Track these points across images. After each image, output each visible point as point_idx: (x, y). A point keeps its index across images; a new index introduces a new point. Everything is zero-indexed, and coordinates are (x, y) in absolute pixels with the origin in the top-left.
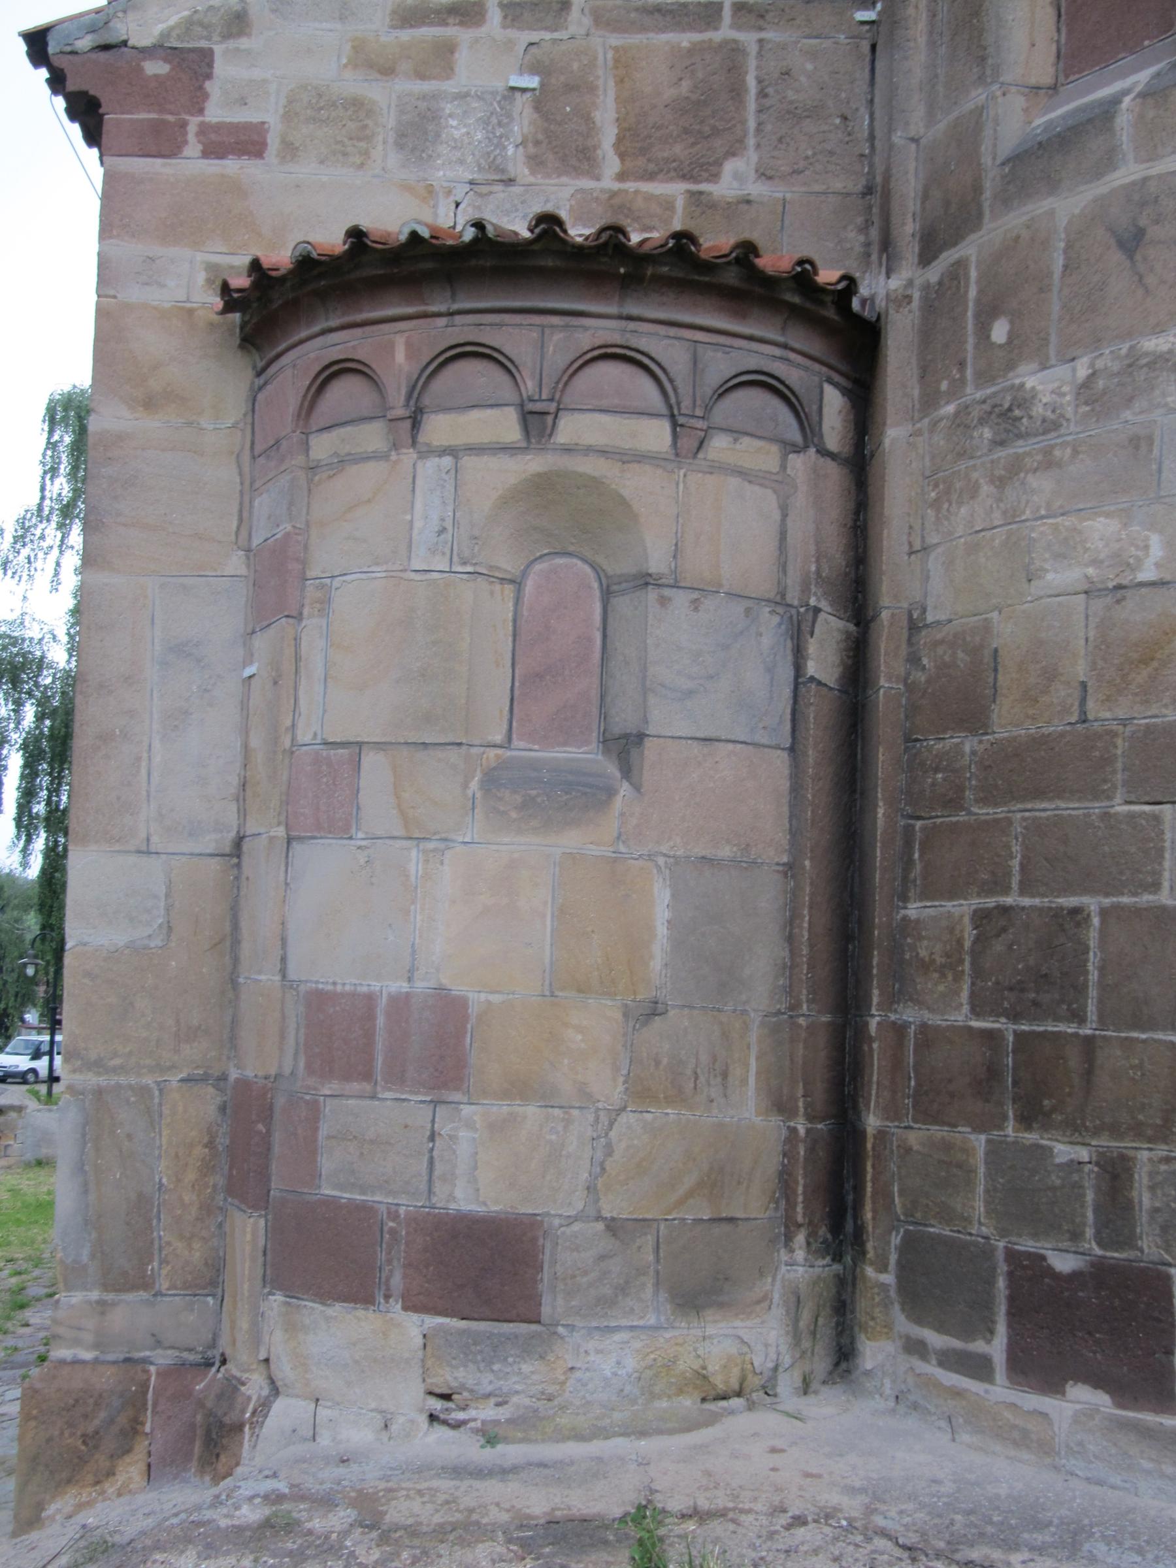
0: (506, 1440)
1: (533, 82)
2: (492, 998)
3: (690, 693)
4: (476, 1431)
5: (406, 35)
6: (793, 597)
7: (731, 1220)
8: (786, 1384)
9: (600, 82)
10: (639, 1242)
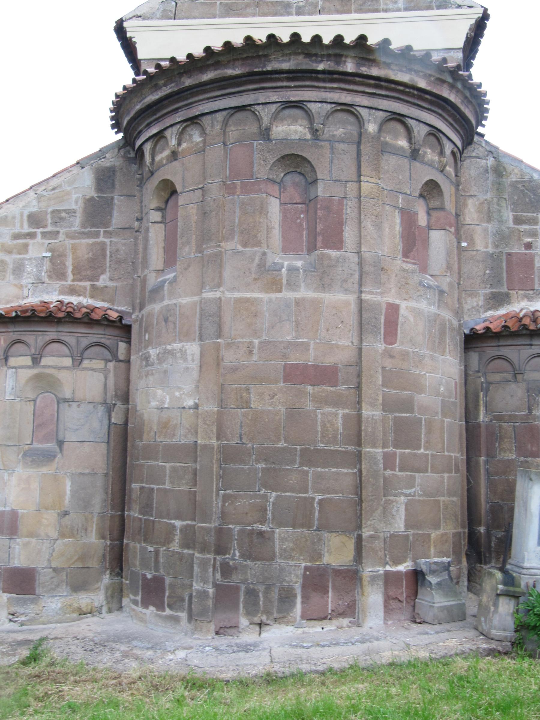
0: (26, 625)
1: (49, 254)
2: (25, 511)
3: (77, 430)
4: (19, 623)
5: (15, 242)
6: (108, 401)
7: (88, 567)
8: (104, 609)
9: (68, 254)
10: (62, 574)
